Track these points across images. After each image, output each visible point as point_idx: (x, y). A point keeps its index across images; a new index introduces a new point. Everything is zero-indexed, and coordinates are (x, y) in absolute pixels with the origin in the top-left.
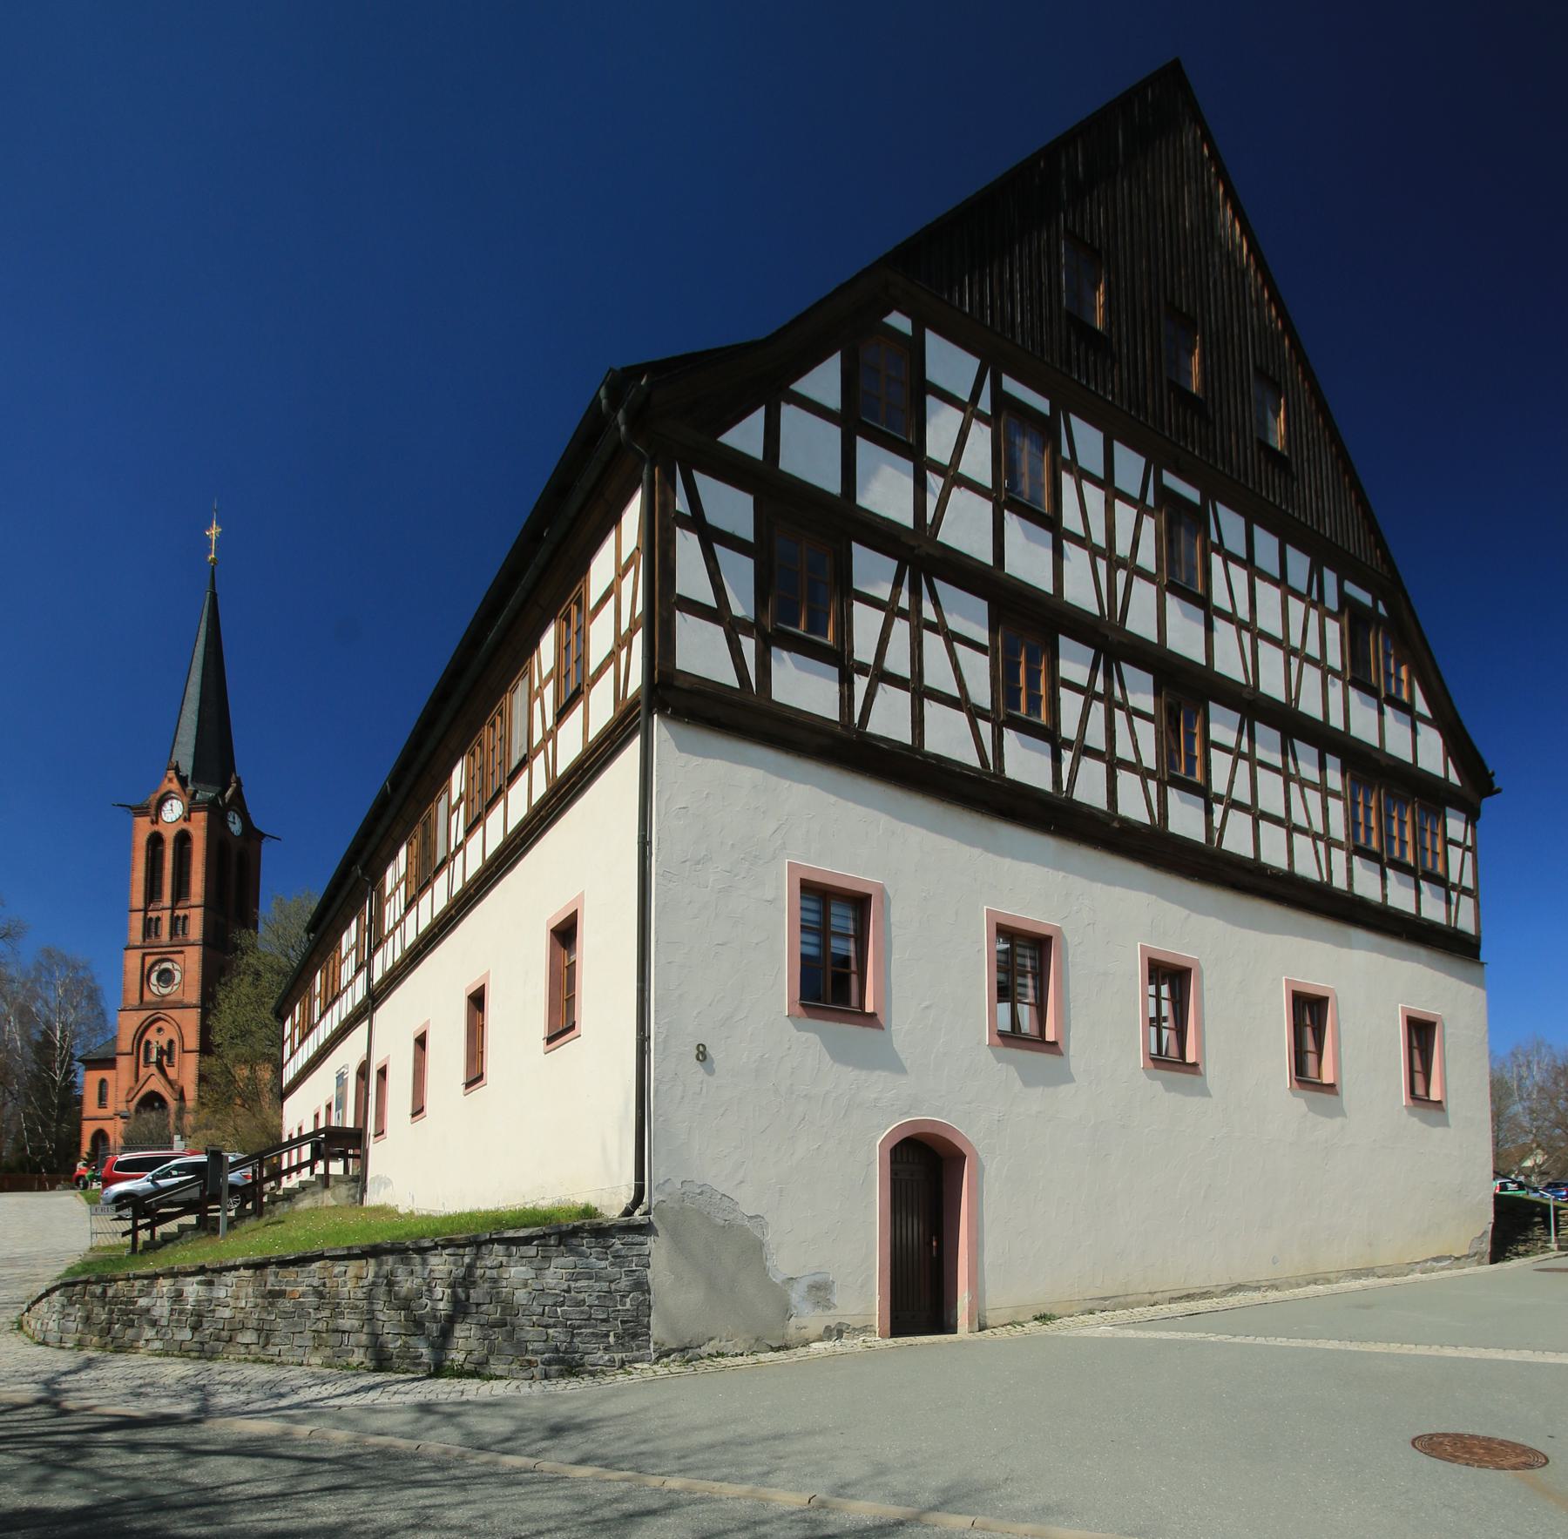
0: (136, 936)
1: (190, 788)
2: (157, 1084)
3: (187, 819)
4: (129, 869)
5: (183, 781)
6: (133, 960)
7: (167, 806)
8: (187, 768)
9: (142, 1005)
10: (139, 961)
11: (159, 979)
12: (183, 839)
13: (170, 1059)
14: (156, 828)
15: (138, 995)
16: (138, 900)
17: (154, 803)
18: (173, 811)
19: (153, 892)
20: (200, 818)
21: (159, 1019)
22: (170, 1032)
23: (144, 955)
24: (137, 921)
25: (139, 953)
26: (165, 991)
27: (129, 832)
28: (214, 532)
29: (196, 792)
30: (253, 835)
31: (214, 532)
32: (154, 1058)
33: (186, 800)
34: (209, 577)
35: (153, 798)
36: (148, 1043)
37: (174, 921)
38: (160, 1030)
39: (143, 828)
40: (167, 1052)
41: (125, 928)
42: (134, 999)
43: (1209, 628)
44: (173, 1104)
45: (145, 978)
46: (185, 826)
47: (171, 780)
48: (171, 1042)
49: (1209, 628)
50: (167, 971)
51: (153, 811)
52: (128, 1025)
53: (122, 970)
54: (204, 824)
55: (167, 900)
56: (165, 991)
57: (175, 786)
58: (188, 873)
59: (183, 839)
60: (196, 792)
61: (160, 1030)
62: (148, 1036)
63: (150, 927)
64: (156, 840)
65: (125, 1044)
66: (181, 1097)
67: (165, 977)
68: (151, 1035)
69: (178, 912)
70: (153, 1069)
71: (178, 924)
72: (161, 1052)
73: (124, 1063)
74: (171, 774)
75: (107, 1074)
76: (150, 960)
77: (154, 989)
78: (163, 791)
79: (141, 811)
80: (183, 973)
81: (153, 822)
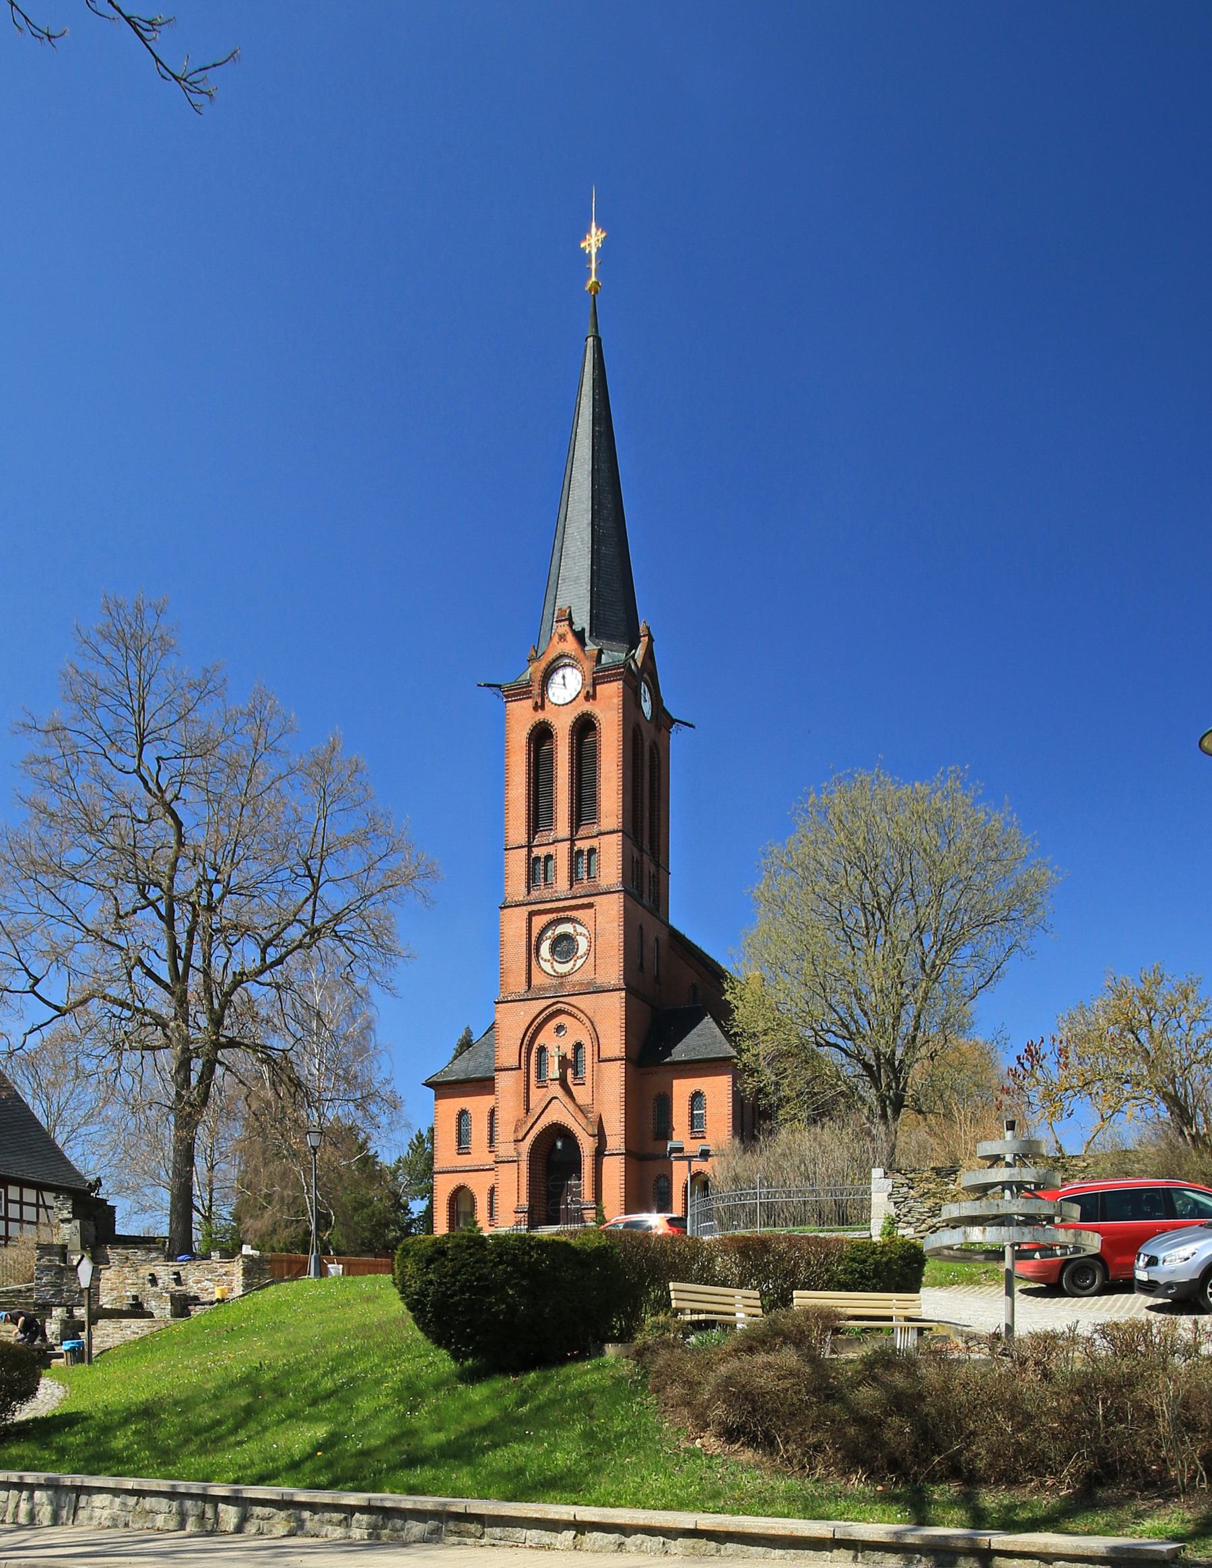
0: (516, 886)
1: (591, 647)
2: (560, 1113)
3: (590, 696)
4: (501, 782)
5: (579, 636)
6: (514, 924)
7: (557, 678)
8: (582, 620)
9: (531, 993)
10: (524, 925)
11: (553, 950)
12: (585, 727)
13: (576, 1073)
14: (541, 716)
15: (524, 978)
16: (517, 830)
17: (539, 675)
18: (567, 687)
19: (538, 817)
20: (612, 691)
21: (560, 1012)
22: (576, 1032)
23: (531, 914)
24: (517, 864)
25: (524, 910)
26: (563, 969)
27: (501, 721)
28: (593, 241)
29: (600, 652)
30: (663, 719)
31: (593, 241)
32: (554, 1071)
33: (589, 665)
34: (592, 310)
35: (534, 671)
36: (542, 1049)
37: (575, 856)
38: (560, 1028)
39: (522, 717)
40: (571, 1063)
41: (499, 875)
42: (517, 983)
43: (56, 1008)
44: (587, 1146)
45: (532, 950)
46: (587, 707)
47: (562, 638)
48: (578, 1047)
49: (56, 1008)
50: (566, 937)
51: (536, 690)
52: (513, 1022)
53: (496, 942)
54: (617, 701)
55: (562, 826)
56: (563, 969)
57: (570, 645)
58: (594, 783)
59: (585, 727)
60: (600, 652)
61: (560, 1028)
62: (540, 1041)
63: (537, 870)
64: (541, 735)
65: (508, 1053)
66: (601, 1136)
67: (564, 946)
68: (546, 1037)
69: (580, 845)
70: (556, 1090)
71: (582, 861)
72: (564, 1062)
73: (507, 1083)
74: (563, 628)
75: (478, 1106)
76: (539, 922)
77: (546, 966)
78: (552, 655)
79: (521, 692)
80: (593, 941)
81: (536, 708)
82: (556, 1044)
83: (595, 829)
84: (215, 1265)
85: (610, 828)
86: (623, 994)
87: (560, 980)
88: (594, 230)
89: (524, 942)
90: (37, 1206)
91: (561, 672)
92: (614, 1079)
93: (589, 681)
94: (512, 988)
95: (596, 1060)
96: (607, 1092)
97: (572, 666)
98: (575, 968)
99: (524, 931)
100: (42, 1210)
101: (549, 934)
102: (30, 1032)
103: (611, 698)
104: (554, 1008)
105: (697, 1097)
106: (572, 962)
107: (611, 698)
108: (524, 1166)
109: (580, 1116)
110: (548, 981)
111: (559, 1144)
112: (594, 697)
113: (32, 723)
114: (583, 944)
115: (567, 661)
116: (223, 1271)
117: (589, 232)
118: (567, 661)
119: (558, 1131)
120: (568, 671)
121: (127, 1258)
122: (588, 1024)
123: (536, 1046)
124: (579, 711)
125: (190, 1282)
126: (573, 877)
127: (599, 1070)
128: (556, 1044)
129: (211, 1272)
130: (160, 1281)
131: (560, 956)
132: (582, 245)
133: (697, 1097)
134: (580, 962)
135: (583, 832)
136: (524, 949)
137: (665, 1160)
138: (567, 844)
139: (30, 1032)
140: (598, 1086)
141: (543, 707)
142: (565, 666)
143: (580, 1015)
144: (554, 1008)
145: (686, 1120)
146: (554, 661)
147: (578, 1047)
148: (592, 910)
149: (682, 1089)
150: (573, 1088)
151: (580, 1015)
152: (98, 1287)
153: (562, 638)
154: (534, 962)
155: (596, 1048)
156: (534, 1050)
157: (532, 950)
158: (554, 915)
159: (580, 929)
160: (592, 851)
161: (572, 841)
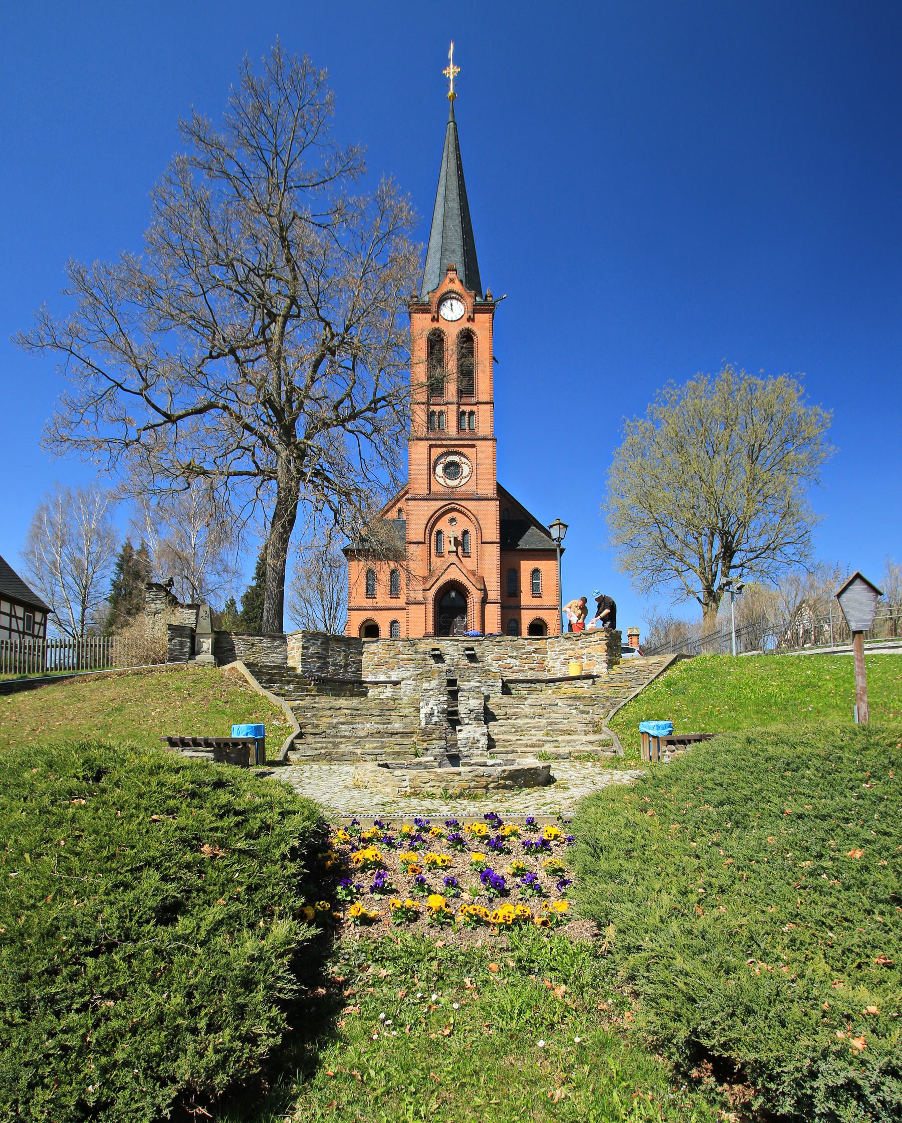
2: (454, 574)
3: (470, 319)
10: (426, 452)
12: (467, 337)
14: (436, 325)
22: (463, 523)
23: (431, 446)
25: (426, 444)
38: (453, 520)
39: (422, 324)
40: (461, 543)
43: (165, 414)
45: (432, 469)
46: (469, 325)
47: (452, 281)
48: (465, 533)
49: (165, 414)
51: (434, 308)
59: (467, 337)
61: (453, 520)
62: (438, 526)
65: (416, 531)
68: (442, 525)
79: (424, 309)
82: (450, 531)
83: (474, 400)
84: (521, 641)
85: (486, 400)
86: (498, 503)
87: (451, 490)
88: (451, 66)
89: (426, 463)
90: (10, 616)
91: (449, 302)
92: (493, 554)
93: (470, 309)
94: (418, 492)
95: (479, 542)
96: (489, 563)
97: (457, 299)
98: (463, 483)
99: (426, 456)
100: (14, 620)
101: (442, 460)
102: (145, 429)
103: (485, 322)
104: (449, 506)
105: (536, 572)
107: (485, 322)
108: (430, 607)
109: (471, 577)
110: (443, 490)
111: (453, 594)
112: (473, 320)
113: (196, 129)
114: (466, 470)
115: (454, 295)
116: (532, 648)
117: (449, 65)
118: (454, 295)
119: (454, 586)
120: (454, 302)
121: (253, 645)
122: (473, 519)
123: (435, 530)
125: (489, 659)
126: (460, 428)
127: (481, 549)
128: (450, 531)
129: (517, 649)
130: (447, 658)
131: (449, 474)
132: (444, 72)
133: (536, 572)
134: (464, 481)
135: (463, 401)
136: (426, 467)
137: (519, 608)
138: (454, 407)
139: (145, 429)
140: (481, 559)
141: (437, 320)
142: (453, 298)
143: (468, 513)
144: (449, 506)
145: (529, 586)
146: (446, 293)
147: (465, 533)
148: (474, 449)
149: (526, 567)
150: (462, 559)
151: (468, 513)
152: (360, 661)
153: (452, 281)
154: (432, 477)
155: (479, 535)
156: (434, 533)
157: (432, 469)
158: (445, 449)
159: (464, 460)
160: (472, 413)
161: (459, 404)
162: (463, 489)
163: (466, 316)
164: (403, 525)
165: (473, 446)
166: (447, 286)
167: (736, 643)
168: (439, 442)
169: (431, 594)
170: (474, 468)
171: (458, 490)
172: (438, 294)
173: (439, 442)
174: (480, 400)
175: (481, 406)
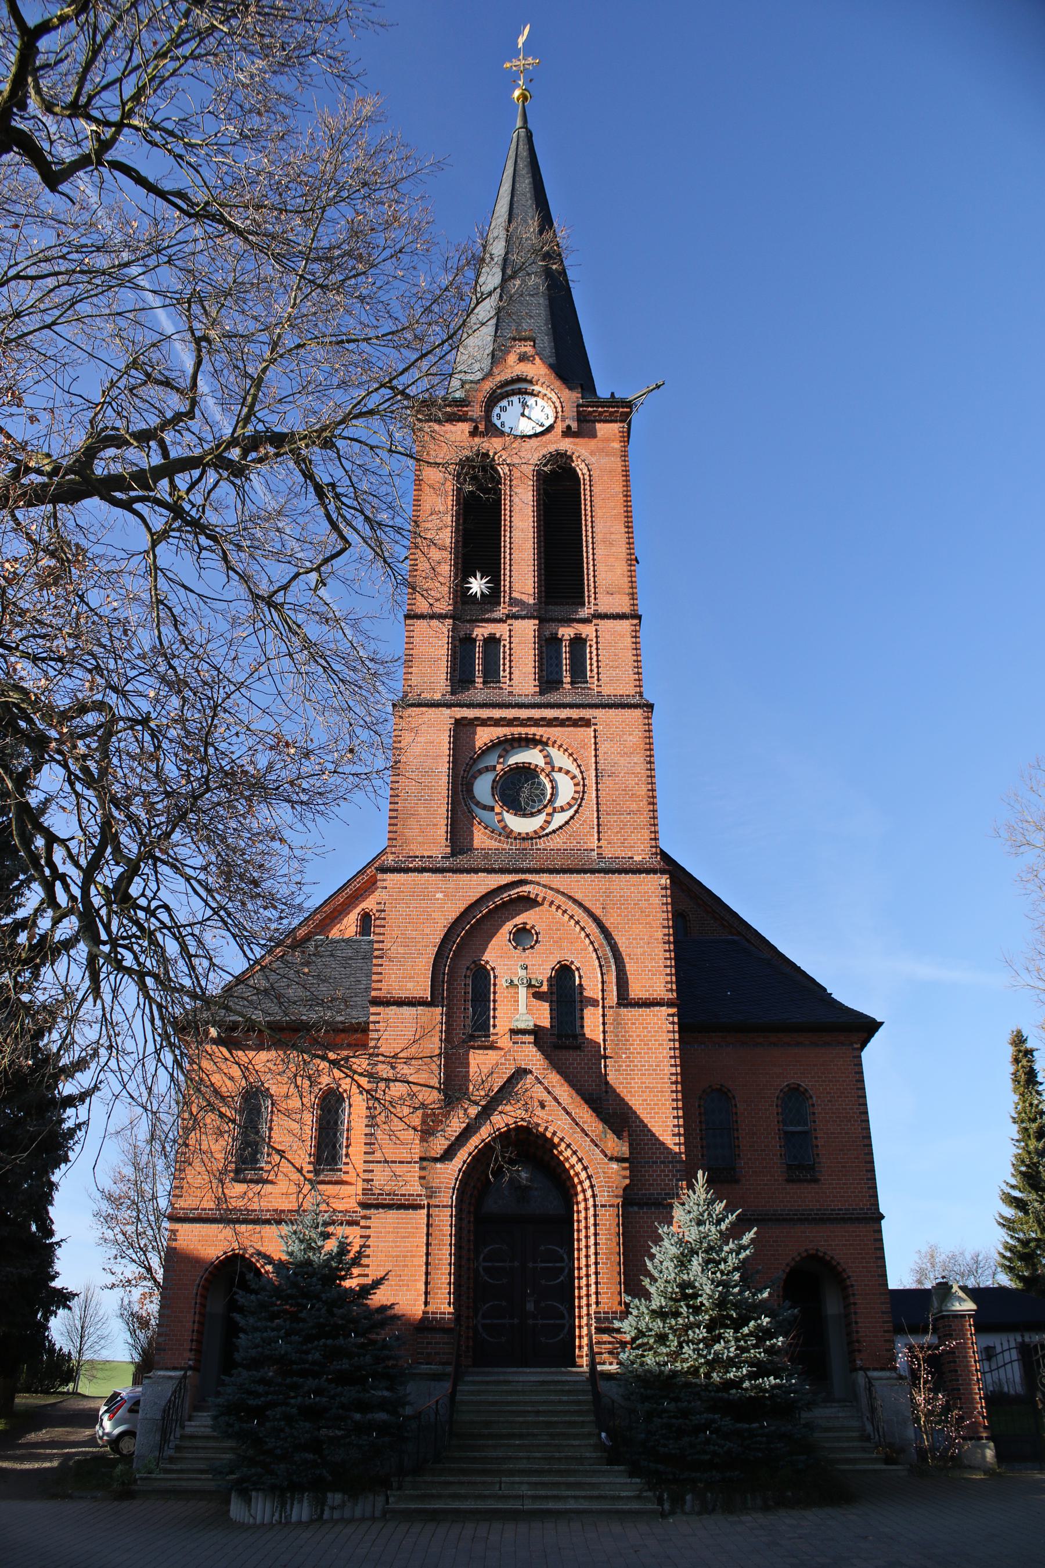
46: (566, 445)
106: (540, 819)
108: (445, 1221)
124: (552, 448)
127: (618, 1023)
132: (42, 820)
134: (559, 819)
146: (508, 383)
155: (612, 977)
162: (557, 842)
163: (560, 428)
164: (364, 953)
165: (586, 723)
166: (513, 367)
167: (170, 1377)
168: (497, 713)
169: (449, 1173)
170: (591, 781)
171: (541, 844)
172: (488, 386)
173: (497, 713)
174: (602, 610)
175: (605, 625)
